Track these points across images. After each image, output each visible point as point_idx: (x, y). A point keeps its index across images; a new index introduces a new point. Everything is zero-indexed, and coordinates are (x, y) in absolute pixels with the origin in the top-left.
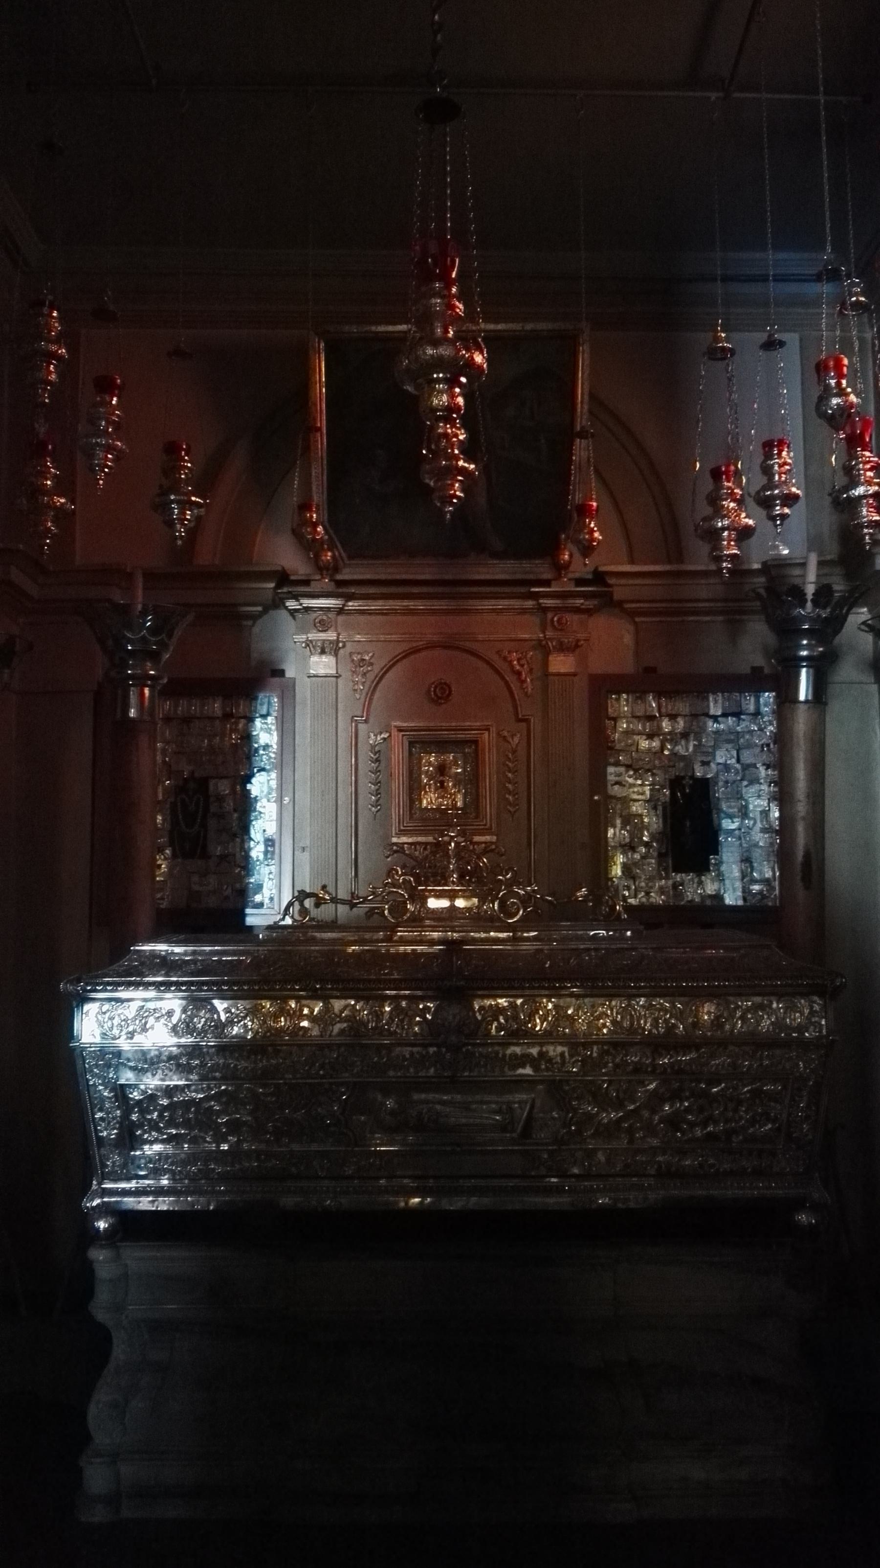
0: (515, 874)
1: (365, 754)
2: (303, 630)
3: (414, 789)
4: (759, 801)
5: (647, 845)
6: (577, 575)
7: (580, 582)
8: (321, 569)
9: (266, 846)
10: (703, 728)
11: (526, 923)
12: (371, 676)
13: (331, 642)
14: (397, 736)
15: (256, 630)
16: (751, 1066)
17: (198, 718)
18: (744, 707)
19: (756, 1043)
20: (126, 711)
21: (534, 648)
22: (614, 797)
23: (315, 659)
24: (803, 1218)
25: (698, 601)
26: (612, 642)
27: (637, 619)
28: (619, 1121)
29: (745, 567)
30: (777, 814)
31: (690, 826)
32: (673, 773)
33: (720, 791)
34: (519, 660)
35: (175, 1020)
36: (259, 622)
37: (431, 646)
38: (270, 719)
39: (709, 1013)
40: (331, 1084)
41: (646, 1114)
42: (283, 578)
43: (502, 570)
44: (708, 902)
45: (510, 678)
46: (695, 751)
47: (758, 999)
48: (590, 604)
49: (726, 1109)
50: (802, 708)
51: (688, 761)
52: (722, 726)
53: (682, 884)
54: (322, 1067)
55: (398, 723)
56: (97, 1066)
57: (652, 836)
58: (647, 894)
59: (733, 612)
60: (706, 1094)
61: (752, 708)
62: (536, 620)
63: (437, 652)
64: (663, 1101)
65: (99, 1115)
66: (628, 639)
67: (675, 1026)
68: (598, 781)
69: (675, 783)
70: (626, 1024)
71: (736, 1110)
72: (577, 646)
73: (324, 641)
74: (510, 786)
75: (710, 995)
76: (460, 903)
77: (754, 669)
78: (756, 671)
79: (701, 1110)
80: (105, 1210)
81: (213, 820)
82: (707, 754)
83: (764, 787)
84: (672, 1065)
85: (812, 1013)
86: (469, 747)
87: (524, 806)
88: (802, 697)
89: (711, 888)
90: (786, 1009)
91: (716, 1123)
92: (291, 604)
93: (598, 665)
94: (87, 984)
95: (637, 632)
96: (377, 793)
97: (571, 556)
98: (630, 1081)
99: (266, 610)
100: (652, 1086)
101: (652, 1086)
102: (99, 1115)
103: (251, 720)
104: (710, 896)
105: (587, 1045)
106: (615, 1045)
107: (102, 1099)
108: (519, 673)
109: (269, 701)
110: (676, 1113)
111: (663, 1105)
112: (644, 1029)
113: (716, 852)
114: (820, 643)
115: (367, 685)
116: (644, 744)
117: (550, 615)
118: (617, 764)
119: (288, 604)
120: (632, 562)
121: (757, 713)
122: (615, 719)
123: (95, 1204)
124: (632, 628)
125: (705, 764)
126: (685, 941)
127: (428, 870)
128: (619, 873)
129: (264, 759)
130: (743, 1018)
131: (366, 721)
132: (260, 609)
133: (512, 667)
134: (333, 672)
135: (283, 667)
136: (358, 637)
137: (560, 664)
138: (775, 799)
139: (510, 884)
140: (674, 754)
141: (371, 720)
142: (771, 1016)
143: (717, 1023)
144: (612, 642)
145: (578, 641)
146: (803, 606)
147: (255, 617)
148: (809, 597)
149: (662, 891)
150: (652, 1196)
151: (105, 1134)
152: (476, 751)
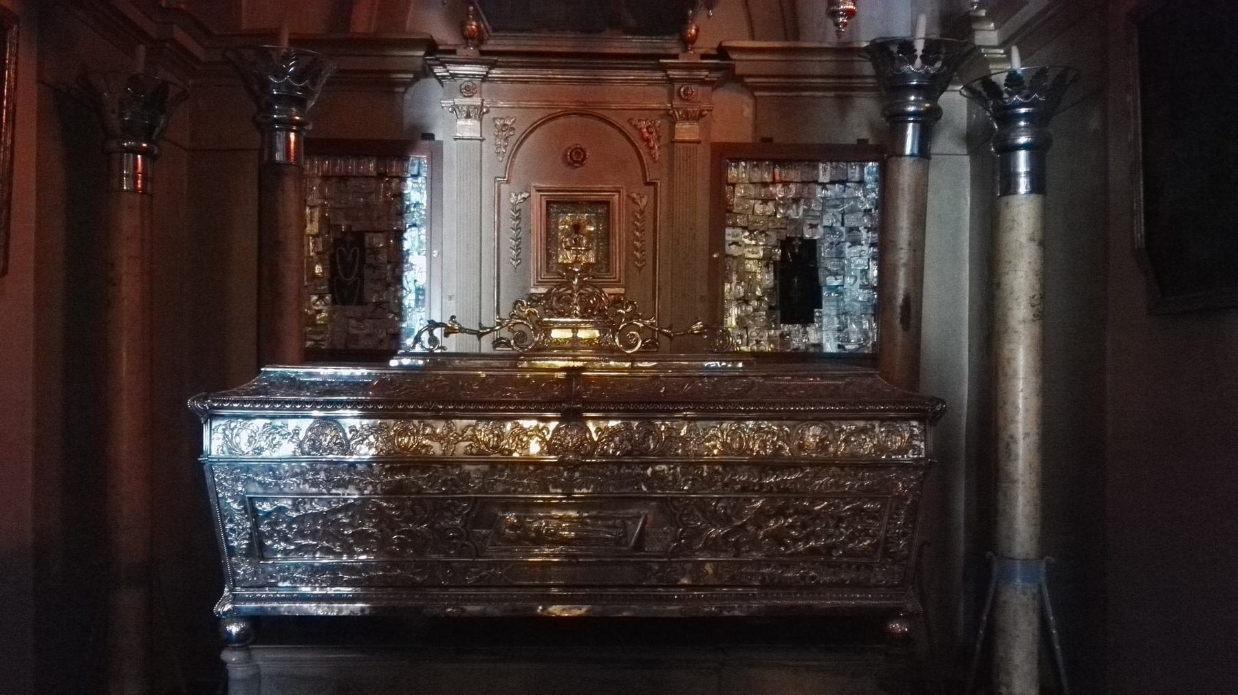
0: (634, 309)
1: (506, 211)
2: (450, 95)
3: (550, 240)
4: (860, 258)
5: (759, 299)
6: (702, 51)
7: (704, 56)
8: (467, 38)
9: (417, 295)
10: (812, 195)
11: (644, 354)
12: (513, 140)
13: (476, 107)
14: (536, 196)
15: (407, 97)
16: (851, 487)
17: (355, 177)
18: (850, 175)
19: (854, 464)
20: (272, 155)
21: (662, 117)
22: (732, 256)
23: (461, 122)
24: (896, 626)
25: (813, 77)
26: (733, 113)
27: (757, 94)
28: (726, 536)
29: (856, 45)
30: (875, 273)
31: (798, 284)
32: (784, 234)
33: (824, 252)
34: (648, 128)
35: (301, 437)
36: (411, 90)
37: (567, 114)
38: (420, 180)
39: (814, 436)
40: (453, 499)
41: (750, 528)
42: (432, 47)
43: (635, 44)
44: (812, 350)
45: (639, 143)
46: (804, 215)
47: (861, 424)
48: (714, 76)
49: (827, 526)
50: (908, 161)
51: (798, 224)
52: (829, 193)
53: (789, 334)
54: (444, 483)
55: (538, 185)
56: (226, 480)
57: (764, 292)
58: (758, 342)
59: (844, 89)
60: (807, 511)
61: (857, 177)
62: (663, 91)
63: (574, 118)
64: (769, 517)
65: (229, 526)
66: (748, 111)
67: (781, 448)
68: (717, 241)
69: (785, 244)
70: (736, 446)
71: (837, 527)
72: (701, 116)
73: (469, 106)
74: (638, 244)
75: (816, 420)
76: (582, 334)
77: (859, 140)
78: (862, 142)
79: (804, 526)
80: (235, 616)
81: (365, 267)
82: (816, 217)
83: (865, 248)
84: (777, 484)
85: (912, 436)
86: (601, 208)
87: (650, 263)
88: (908, 151)
89: (813, 337)
90: (888, 432)
91: (818, 538)
92: (439, 71)
93: (721, 134)
94: (214, 401)
95: (756, 106)
96: (518, 248)
97: (697, 30)
98: (737, 499)
99: (417, 78)
100: (759, 504)
101: (759, 504)
102: (229, 526)
103: (403, 179)
104: (814, 345)
105: (697, 465)
106: (725, 465)
107: (232, 512)
108: (648, 140)
109: (418, 162)
110: (781, 528)
111: (767, 521)
112: (752, 450)
113: (820, 306)
114: (927, 99)
115: (509, 148)
116: (759, 209)
117: (677, 86)
118: (734, 226)
119: (436, 70)
120: (753, 38)
121: (861, 182)
122: (734, 185)
123: (226, 609)
124: (751, 102)
125: (813, 226)
126: (791, 381)
127: (555, 303)
128: (734, 324)
129: (415, 216)
130: (846, 441)
131: (508, 182)
132: (411, 76)
133: (642, 134)
134: (478, 135)
135: (432, 132)
136: (501, 104)
137: (686, 131)
138: (874, 259)
139: (630, 317)
140: (786, 217)
141: (513, 181)
142: (869, 439)
143: (822, 445)
144: (733, 113)
145: (702, 111)
146: (912, 63)
147: (407, 85)
148: (919, 52)
149: (771, 340)
150: (755, 605)
151: (236, 544)
152: (608, 211)
